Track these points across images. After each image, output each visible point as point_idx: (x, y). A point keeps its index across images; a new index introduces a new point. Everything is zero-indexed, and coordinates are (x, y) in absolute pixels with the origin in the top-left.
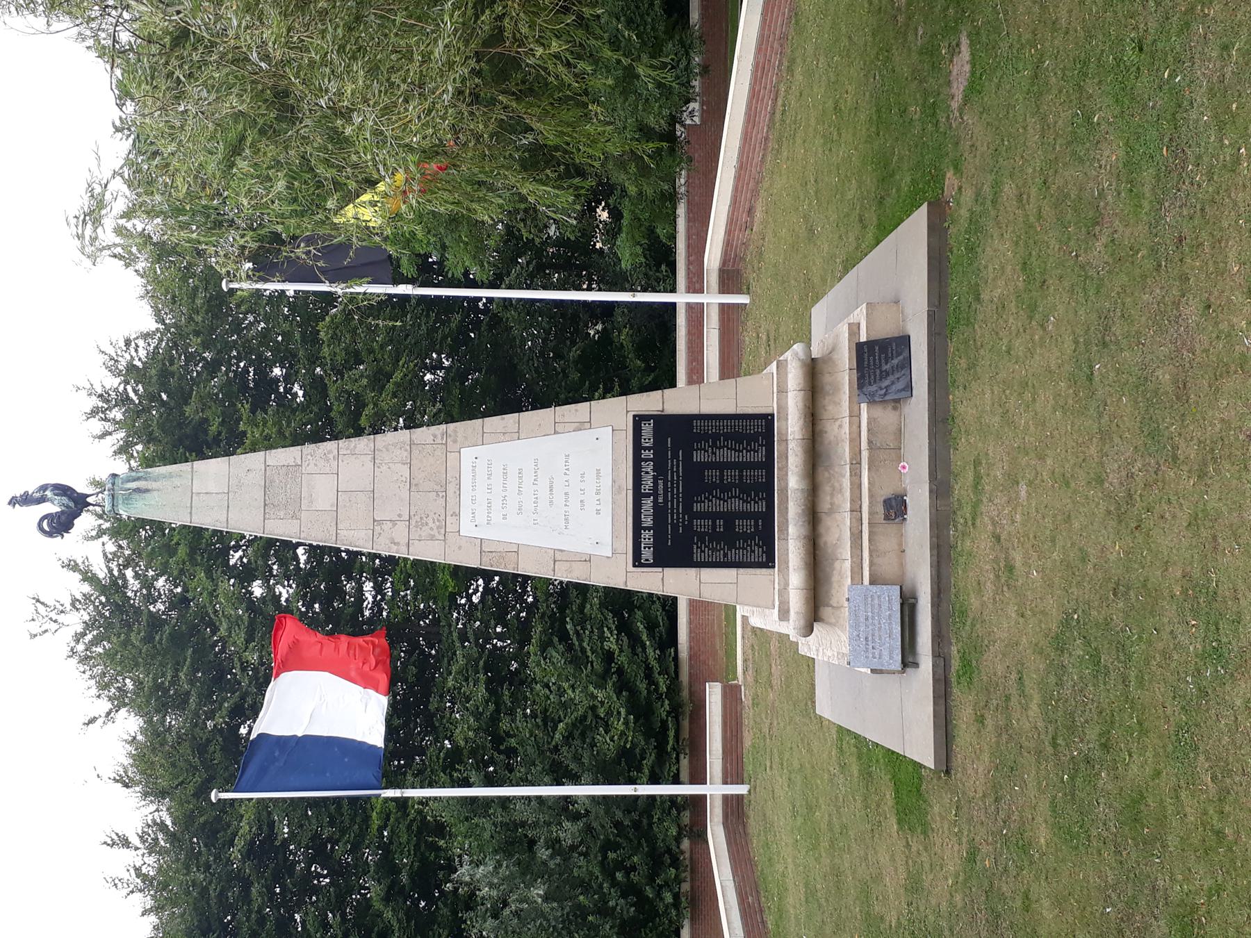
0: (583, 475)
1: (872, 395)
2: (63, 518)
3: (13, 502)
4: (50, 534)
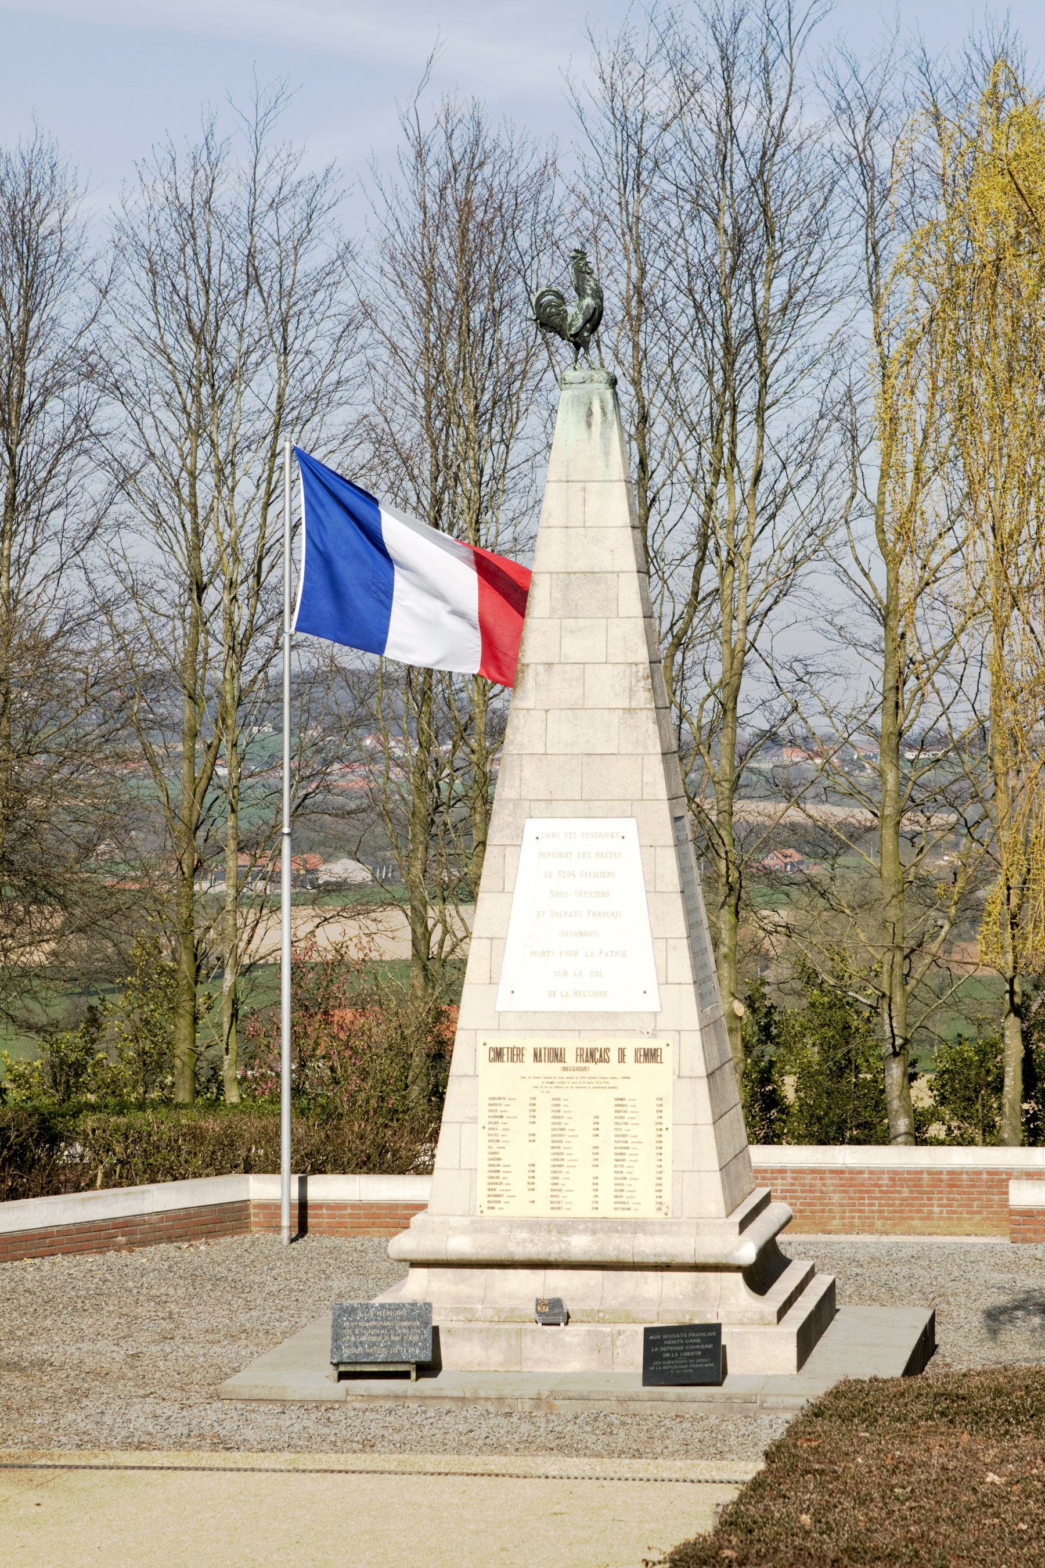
0: (599, 974)
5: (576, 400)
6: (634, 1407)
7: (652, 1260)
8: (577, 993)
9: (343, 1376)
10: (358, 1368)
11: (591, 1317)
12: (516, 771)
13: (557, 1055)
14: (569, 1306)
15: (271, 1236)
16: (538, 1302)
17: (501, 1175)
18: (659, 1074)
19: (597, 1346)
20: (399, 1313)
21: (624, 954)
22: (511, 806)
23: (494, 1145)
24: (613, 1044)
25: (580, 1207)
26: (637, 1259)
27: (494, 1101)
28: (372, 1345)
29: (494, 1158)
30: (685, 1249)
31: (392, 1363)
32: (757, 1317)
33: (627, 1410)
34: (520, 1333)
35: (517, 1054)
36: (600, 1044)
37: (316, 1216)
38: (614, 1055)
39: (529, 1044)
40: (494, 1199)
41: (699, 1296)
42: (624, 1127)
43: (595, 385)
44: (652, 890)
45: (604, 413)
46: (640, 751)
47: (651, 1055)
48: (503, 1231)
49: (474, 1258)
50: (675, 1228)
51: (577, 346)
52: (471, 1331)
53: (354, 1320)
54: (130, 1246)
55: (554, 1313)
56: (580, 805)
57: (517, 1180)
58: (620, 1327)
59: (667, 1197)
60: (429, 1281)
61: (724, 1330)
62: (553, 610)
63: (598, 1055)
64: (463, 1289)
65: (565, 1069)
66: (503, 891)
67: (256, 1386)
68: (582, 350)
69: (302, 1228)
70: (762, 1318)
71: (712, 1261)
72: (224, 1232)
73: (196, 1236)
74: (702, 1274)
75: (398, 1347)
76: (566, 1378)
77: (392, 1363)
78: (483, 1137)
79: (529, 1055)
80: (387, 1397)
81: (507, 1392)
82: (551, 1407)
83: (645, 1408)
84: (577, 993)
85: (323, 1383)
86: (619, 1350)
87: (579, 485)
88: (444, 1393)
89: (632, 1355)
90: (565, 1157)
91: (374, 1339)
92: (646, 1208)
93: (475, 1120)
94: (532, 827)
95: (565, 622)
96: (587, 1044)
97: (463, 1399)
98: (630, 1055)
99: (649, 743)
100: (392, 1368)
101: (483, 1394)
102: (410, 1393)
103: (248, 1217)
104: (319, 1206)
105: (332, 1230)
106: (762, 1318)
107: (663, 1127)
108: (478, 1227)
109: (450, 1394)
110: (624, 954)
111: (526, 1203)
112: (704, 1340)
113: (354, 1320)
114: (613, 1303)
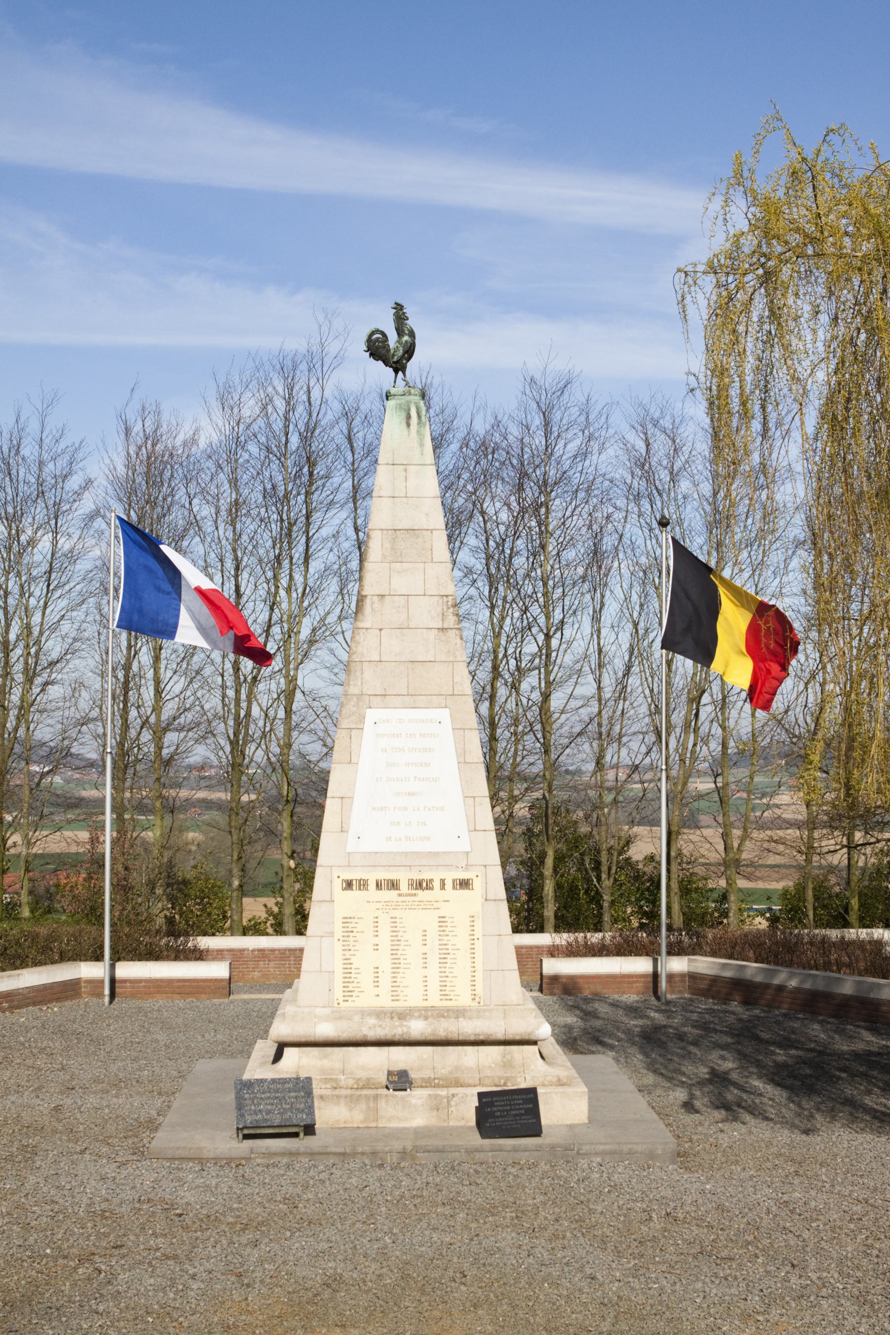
0: (424, 824)
1: (654, 1062)
2: (383, 352)
3: (399, 307)
4: (369, 340)
5: (400, 407)
6: (479, 1156)
7: (472, 1038)
8: (408, 838)
9: (246, 1137)
10: (259, 1131)
11: (428, 1083)
12: (359, 674)
13: (393, 885)
14: (413, 1075)
15: (95, 1000)
16: (390, 1073)
17: (353, 975)
18: (472, 898)
19: (436, 1106)
20: (287, 1086)
21: (442, 809)
22: (355, 699)
23: (347, 953)
24: (436, 876)
25: (413, 998)
26: (461, 1038)
27: (347, 920)
28: (269, 1112)
29: (347, 962)
30: (498, 1030)
31: (285, 1126)
32: (555, 1080)
33: (473, 1159)
34: (376, 1098)
35: (363, 884)
36: (426, 876)
37: (122, 987)
38: (437, 884)
39: (372, 877)
40: (348, 993)
41: (507, 1065)
42: (446, 938)
43: (412, 397)
44: (463, 761)
45: (419, 417)
46: (451, 659)
47: (465, 884)
48: (357, 1018)
49: (336, 1040)
50: (487, 1014)
51: (396, 371)
52: (338, 1097)
53: (253, 1092)
54: (11, 1009)
55: (400, 1081)
56: (407, 698)
57: (365, 978)
58: (453, 1090)
59: (479, 990)
60: (300, 1058)
61: (539, 1091)
62: (384, 556)
63: (424, 885)
64: (326, 1063)
65: (400, 895)
66: (350, 762)
67: (178, 1148)
68: (400, 373)
69: (113, 995)
70: (559, 1080)
71: (518, 1038)
72: (66, 998)
73: (50, 1001)
74: (508, 1048)
75: (289, 1114)
76: (418, 1133)
77: (285, 1126)
78: (338, 946)
79: (372, 885)
80: (283, 1154)
81: (379, 1147)
82: (413, 1158)
83: (489, 1157)
84: (408, 838)
85: (228, 1144)
86: (453, 1109)
87: (402, 467)
88: (329, 1150)
89: (466, 1111)
90: (401, 961)
91: (269, 1107)
92: (463, 999)
93: (331, 934)
94: (371, 715)
95: (393, 565)
96: (417, 876)
97: (344, 1154)
98: (449, 884)
99: (458, 653)
100: (284, 1131)
101: (360, 1150)
102: (302, 1150)
103: (80, 988)
104: (124, 981)
105: (133, 996)
106: (559, 1080)
107: (475, 937)
108: (338, 1016)
109: (333, 1150)
110: (442, 809)
111: (370, 997)
112: (526, 1101)
113: (253, 1092)
114: (443, 1071)
